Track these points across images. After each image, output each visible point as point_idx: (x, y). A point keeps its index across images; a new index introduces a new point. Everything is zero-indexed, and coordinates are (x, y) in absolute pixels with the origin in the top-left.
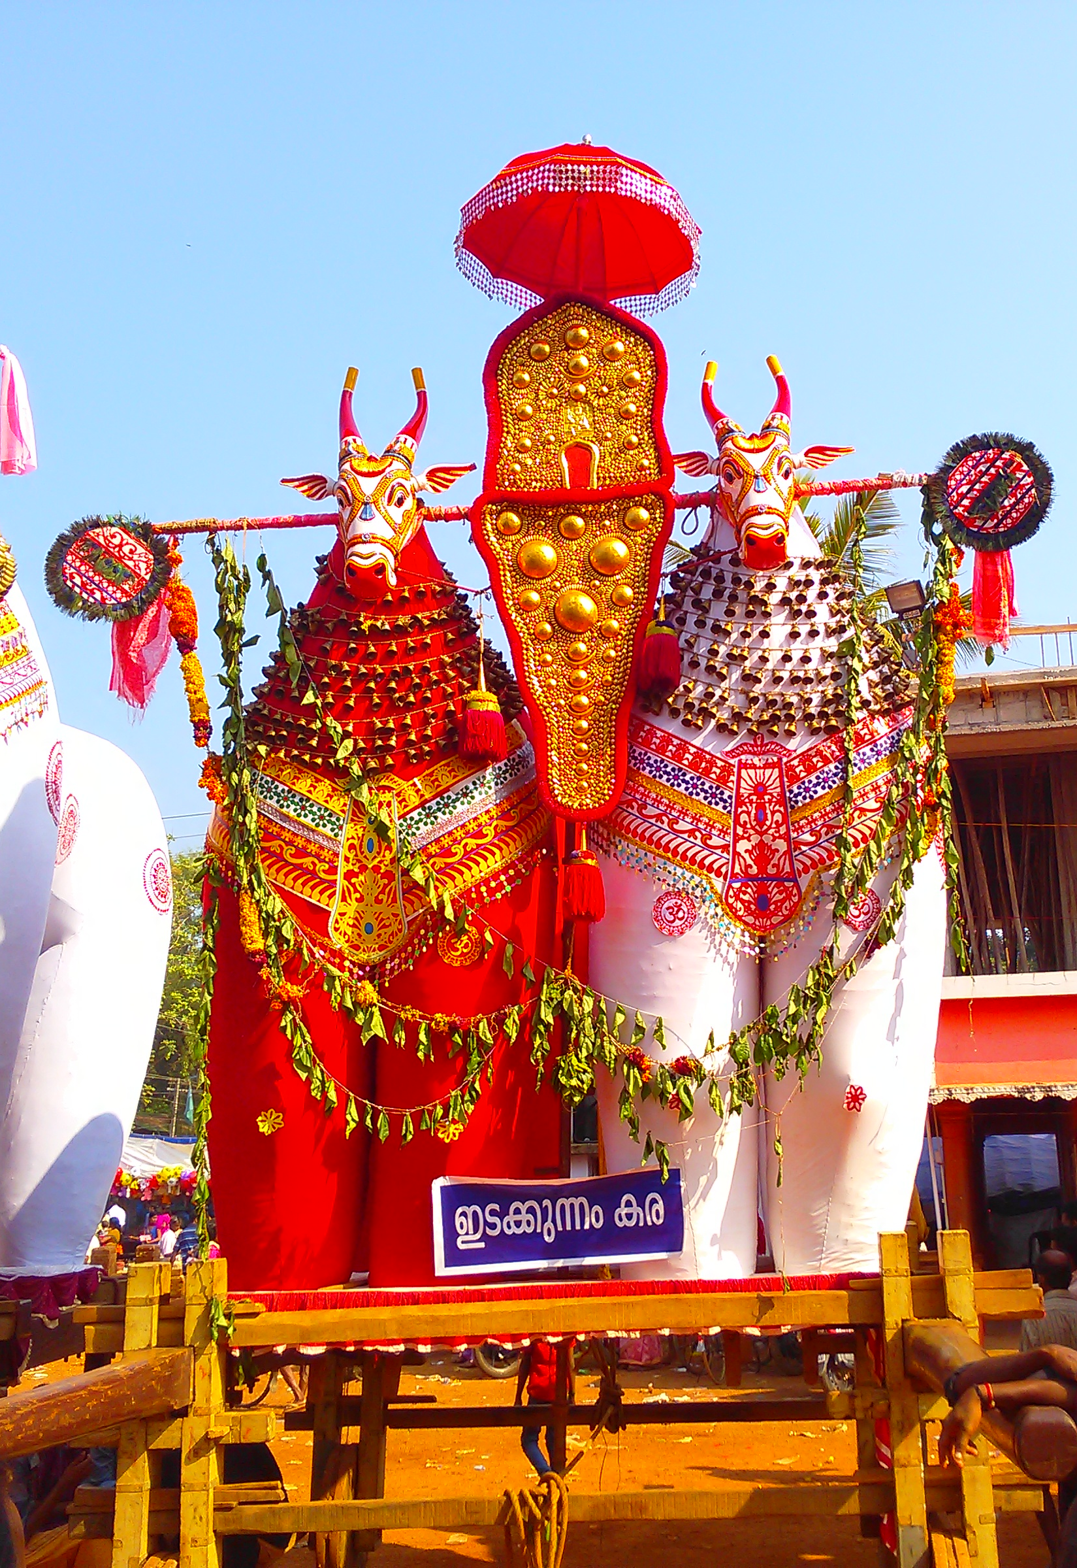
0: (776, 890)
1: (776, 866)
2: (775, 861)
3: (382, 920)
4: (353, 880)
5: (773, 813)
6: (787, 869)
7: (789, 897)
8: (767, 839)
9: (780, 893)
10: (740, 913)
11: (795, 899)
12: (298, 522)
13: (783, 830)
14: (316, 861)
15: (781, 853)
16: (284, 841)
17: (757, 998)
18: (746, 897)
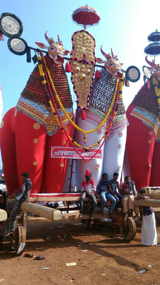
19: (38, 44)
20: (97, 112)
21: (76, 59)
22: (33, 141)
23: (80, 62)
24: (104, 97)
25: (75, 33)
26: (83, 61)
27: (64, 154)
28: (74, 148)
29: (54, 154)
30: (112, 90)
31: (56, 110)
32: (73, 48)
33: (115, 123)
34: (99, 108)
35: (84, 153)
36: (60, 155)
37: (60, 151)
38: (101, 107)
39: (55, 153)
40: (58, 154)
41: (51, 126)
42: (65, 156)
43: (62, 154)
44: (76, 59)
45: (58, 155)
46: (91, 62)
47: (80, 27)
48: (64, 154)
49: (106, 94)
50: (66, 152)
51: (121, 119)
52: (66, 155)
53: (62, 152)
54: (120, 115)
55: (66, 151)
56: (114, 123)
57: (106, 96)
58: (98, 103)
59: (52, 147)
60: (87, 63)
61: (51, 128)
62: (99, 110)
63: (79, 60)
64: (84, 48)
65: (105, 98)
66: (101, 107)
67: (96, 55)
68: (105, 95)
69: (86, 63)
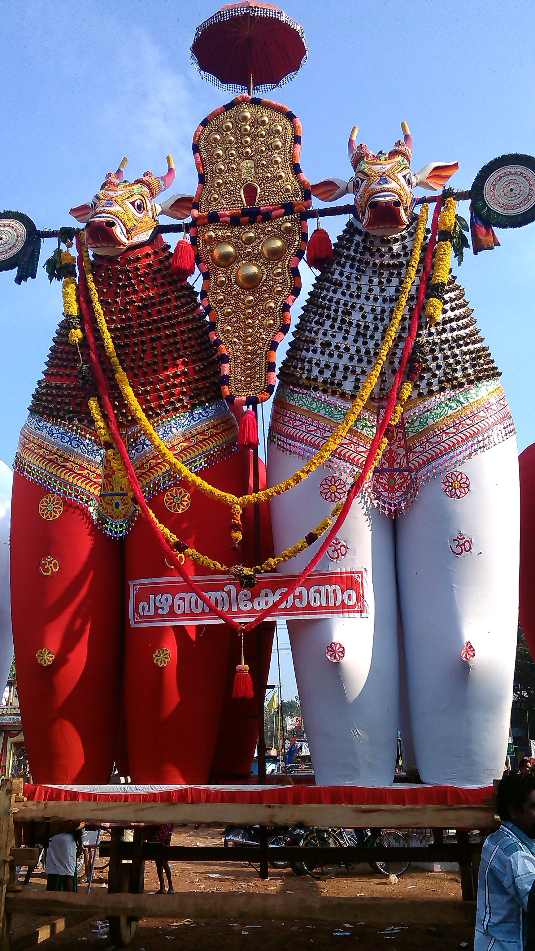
0: (398, 477)
1: (399, 463)
2: (398, 461)
3: (124, 500)
4: (109, 479)
5: (397, 434)
6: (405, 465)
7: (405, 481)
8: (394, 448)
9: (401, 478)
10: (380, 490)
11: (409, 482)
12: (318, 556)
13: (403, 442)
14: (74, 465)
15: (402, 455)
16: (58, 455)
17: (395, 587)
18: (383, 481)
19: (327, 200)
20: (314, 406)
21: (214, 218)
22: (39, 567)
23: (234, 221)
24: (347, 332)
25: (205, 123)
26: (245, 213)
27: (171, 607)
28: (186, 580)
29: (138, 613)
30: (390, 291)
31: (112, 435)
32: (202, 179)
33: (419, 434)
34: (325, 382)
35: (266, 595)
36: (156, 615)
37: (159, 597)
38: (333, 375)
39: (141, 604)
40: (152, 612)
41: (117, 499)
42: (179, 615)
43: (166, 611)
44: (214, 218)
45: (150, 617)
46: (281, 208)
47: (226, 94)
48: (171, 607)
49: (356, 316)
50: (319, 592)
51: (450, 412)
52: (184, 614)
53: (164, 601)
54: (449, 393)
55: (317, 588)
56: (412, 434)
57: (358, 326)
58: (318, 365)
59: (131, 584)
60: (267, 217)
61: (117, 505)
62: (325, 391)
63: (225, 216)
64: (247, 164)
65: (353, 331)
66: (333, 375)
67: (304, 176)
68: (350, 324)
69: (260, 217)
